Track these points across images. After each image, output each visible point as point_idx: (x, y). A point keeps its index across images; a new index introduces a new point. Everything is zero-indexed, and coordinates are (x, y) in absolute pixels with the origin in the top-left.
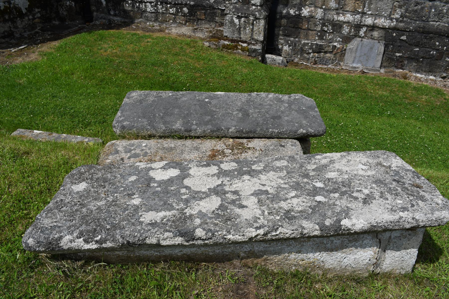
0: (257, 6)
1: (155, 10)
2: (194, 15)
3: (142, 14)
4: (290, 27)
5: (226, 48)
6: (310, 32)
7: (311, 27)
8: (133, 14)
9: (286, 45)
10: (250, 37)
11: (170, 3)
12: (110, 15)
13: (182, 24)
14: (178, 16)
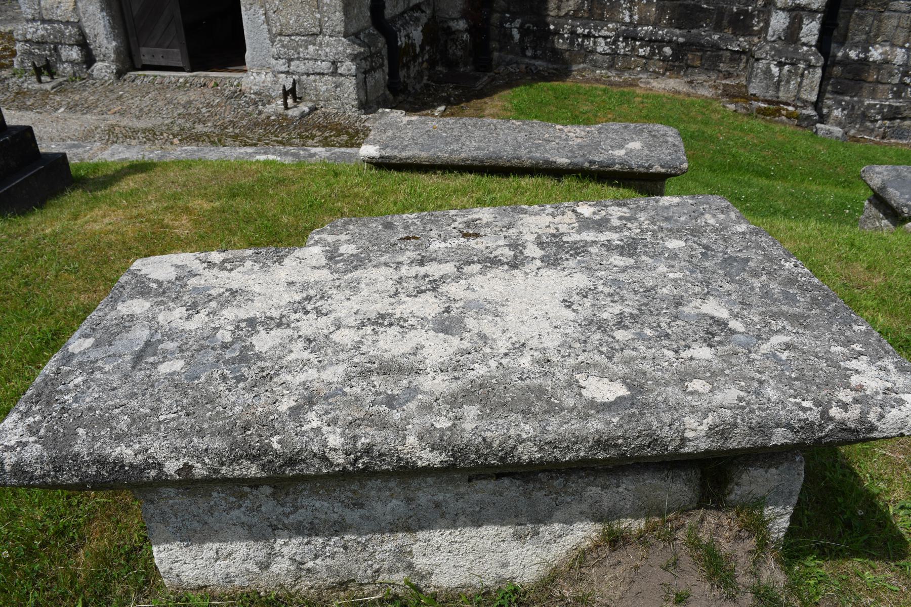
0: (811, 46)
1: (613, 50)
2: (682, 59)
3: (586, 56)
4: (846, 79)
5: (762, 114)
6: (880, 86)
7: (882, 79)
8: (570, 56)
9: (837, 109)
10: (795, 96)
11: (641, 39)
12: (525, 56)
13: (658, 73)
14: (652, 61)
